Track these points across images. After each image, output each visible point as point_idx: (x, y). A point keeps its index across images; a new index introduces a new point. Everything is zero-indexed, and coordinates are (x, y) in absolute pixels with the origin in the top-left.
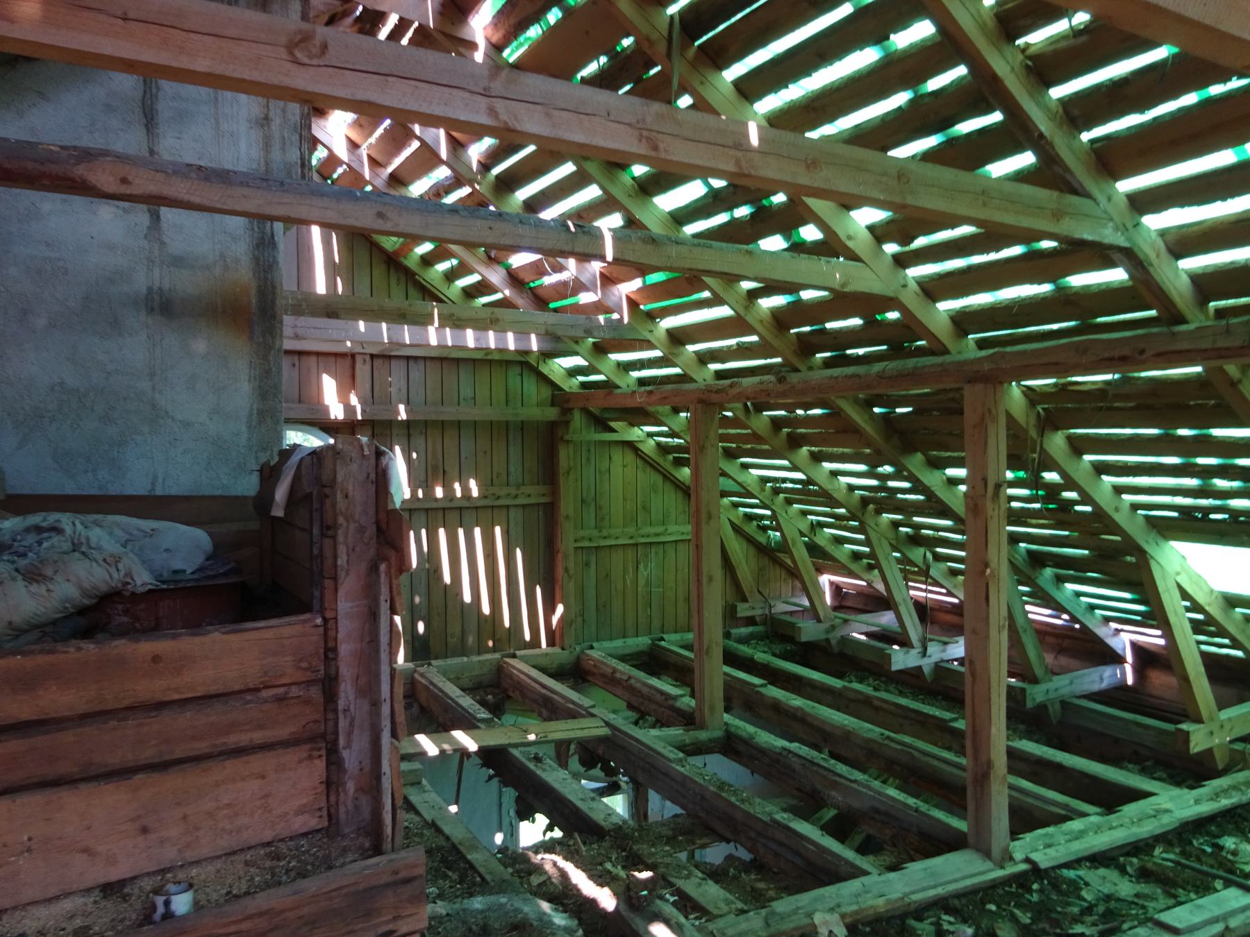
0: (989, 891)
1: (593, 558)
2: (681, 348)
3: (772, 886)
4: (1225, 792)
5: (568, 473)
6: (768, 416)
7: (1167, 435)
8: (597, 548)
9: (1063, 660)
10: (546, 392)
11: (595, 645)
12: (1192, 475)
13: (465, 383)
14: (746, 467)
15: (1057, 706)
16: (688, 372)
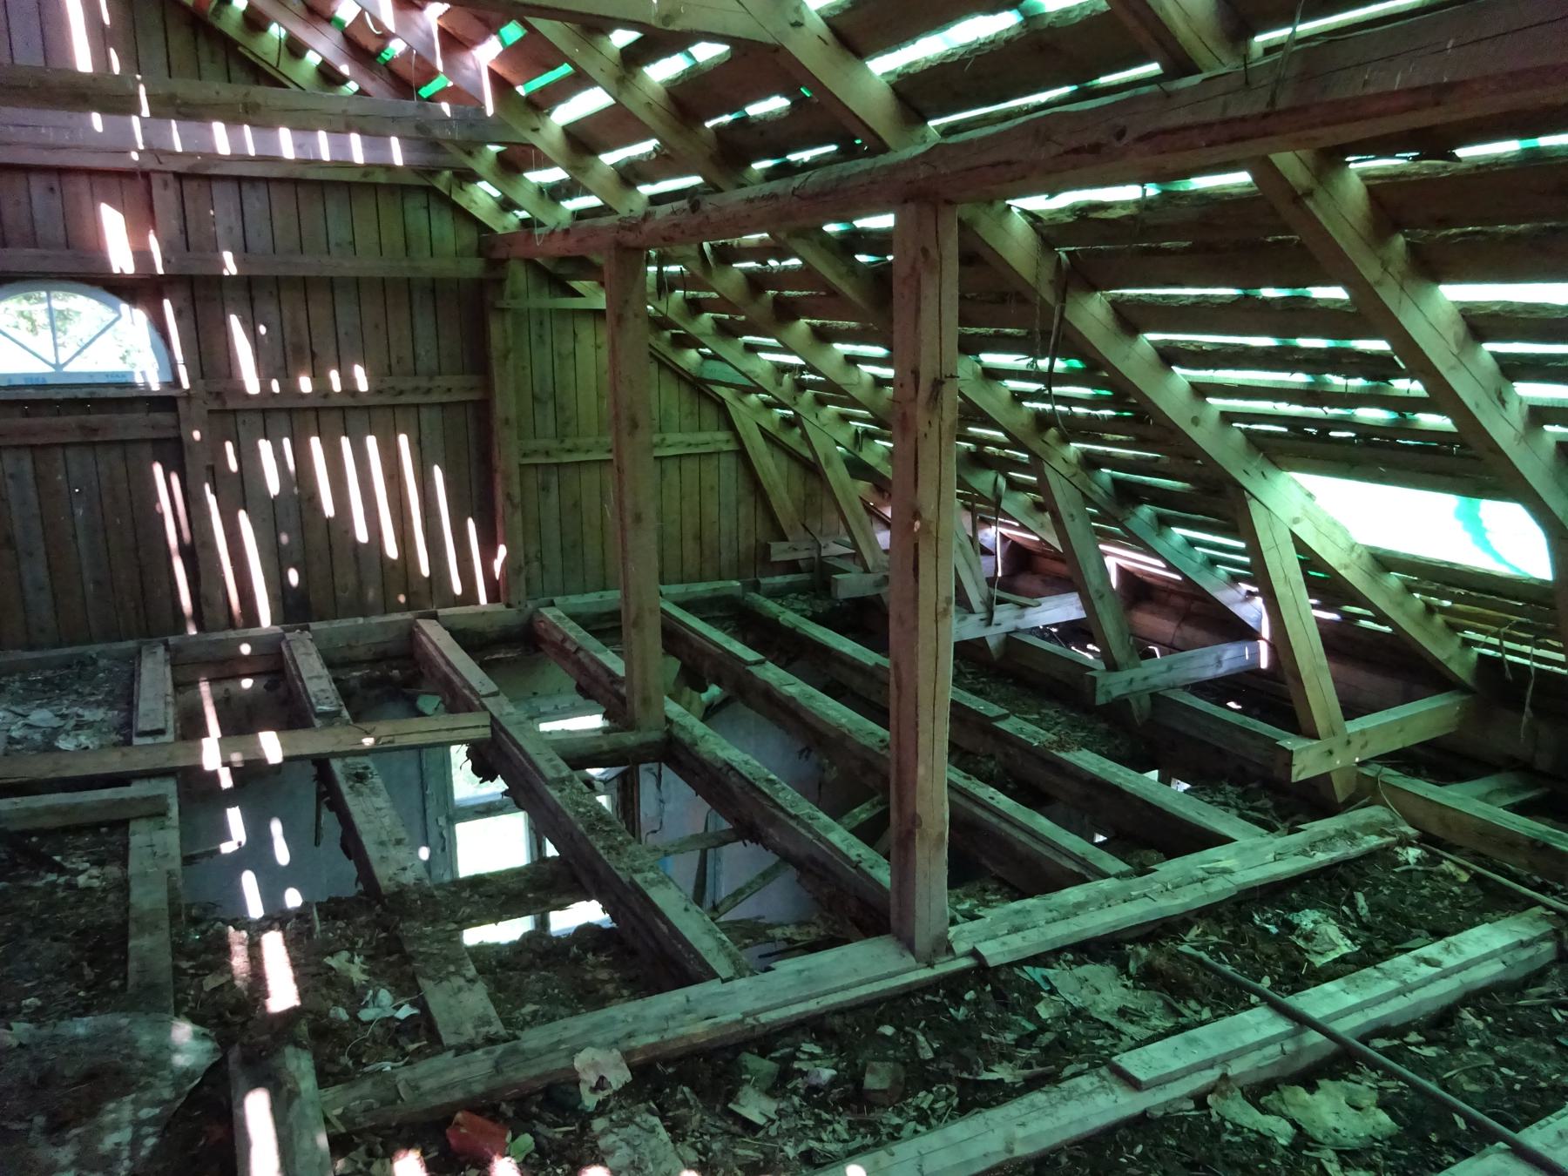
0: (897, 1004)
1: (554, 479)
2: (590, 160)
3: (617, 976)
4: (1327, 841)
5: (506, 357)
6: (741, 269)
7: (1246, 296)
8: (557, 465)
9: (1189, 631)
10: (469, 236)
11: (557, 600)
12: (1292, 367)
13: (337, 220)
14: (752, 349)
15: (1146, 702)
16: (609, 202)
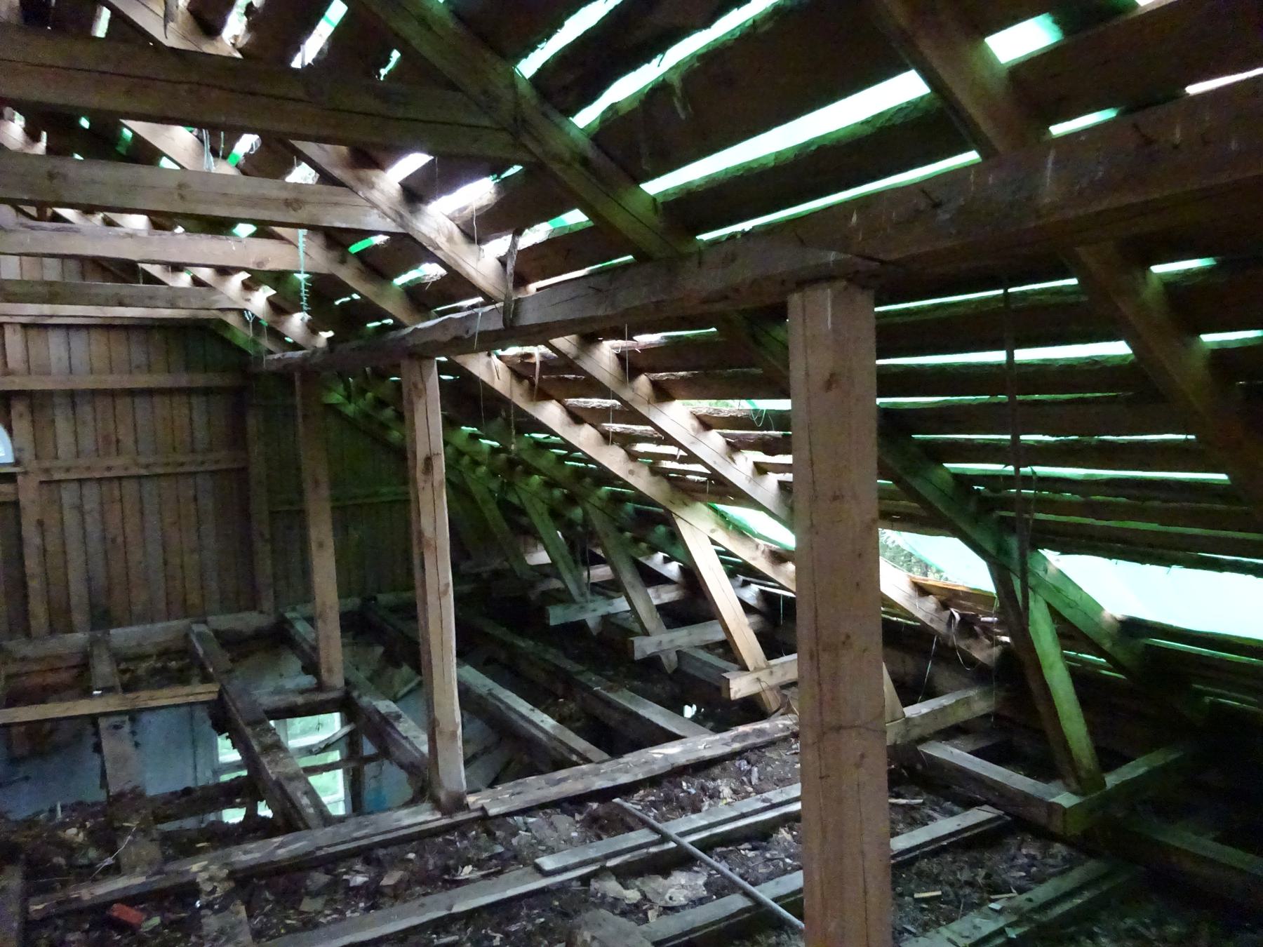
15: (674, 657)
